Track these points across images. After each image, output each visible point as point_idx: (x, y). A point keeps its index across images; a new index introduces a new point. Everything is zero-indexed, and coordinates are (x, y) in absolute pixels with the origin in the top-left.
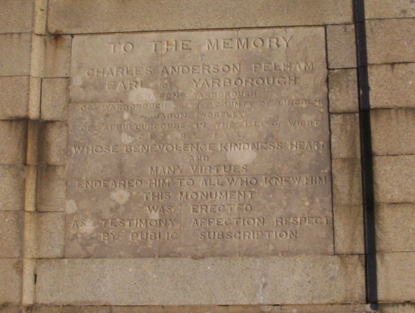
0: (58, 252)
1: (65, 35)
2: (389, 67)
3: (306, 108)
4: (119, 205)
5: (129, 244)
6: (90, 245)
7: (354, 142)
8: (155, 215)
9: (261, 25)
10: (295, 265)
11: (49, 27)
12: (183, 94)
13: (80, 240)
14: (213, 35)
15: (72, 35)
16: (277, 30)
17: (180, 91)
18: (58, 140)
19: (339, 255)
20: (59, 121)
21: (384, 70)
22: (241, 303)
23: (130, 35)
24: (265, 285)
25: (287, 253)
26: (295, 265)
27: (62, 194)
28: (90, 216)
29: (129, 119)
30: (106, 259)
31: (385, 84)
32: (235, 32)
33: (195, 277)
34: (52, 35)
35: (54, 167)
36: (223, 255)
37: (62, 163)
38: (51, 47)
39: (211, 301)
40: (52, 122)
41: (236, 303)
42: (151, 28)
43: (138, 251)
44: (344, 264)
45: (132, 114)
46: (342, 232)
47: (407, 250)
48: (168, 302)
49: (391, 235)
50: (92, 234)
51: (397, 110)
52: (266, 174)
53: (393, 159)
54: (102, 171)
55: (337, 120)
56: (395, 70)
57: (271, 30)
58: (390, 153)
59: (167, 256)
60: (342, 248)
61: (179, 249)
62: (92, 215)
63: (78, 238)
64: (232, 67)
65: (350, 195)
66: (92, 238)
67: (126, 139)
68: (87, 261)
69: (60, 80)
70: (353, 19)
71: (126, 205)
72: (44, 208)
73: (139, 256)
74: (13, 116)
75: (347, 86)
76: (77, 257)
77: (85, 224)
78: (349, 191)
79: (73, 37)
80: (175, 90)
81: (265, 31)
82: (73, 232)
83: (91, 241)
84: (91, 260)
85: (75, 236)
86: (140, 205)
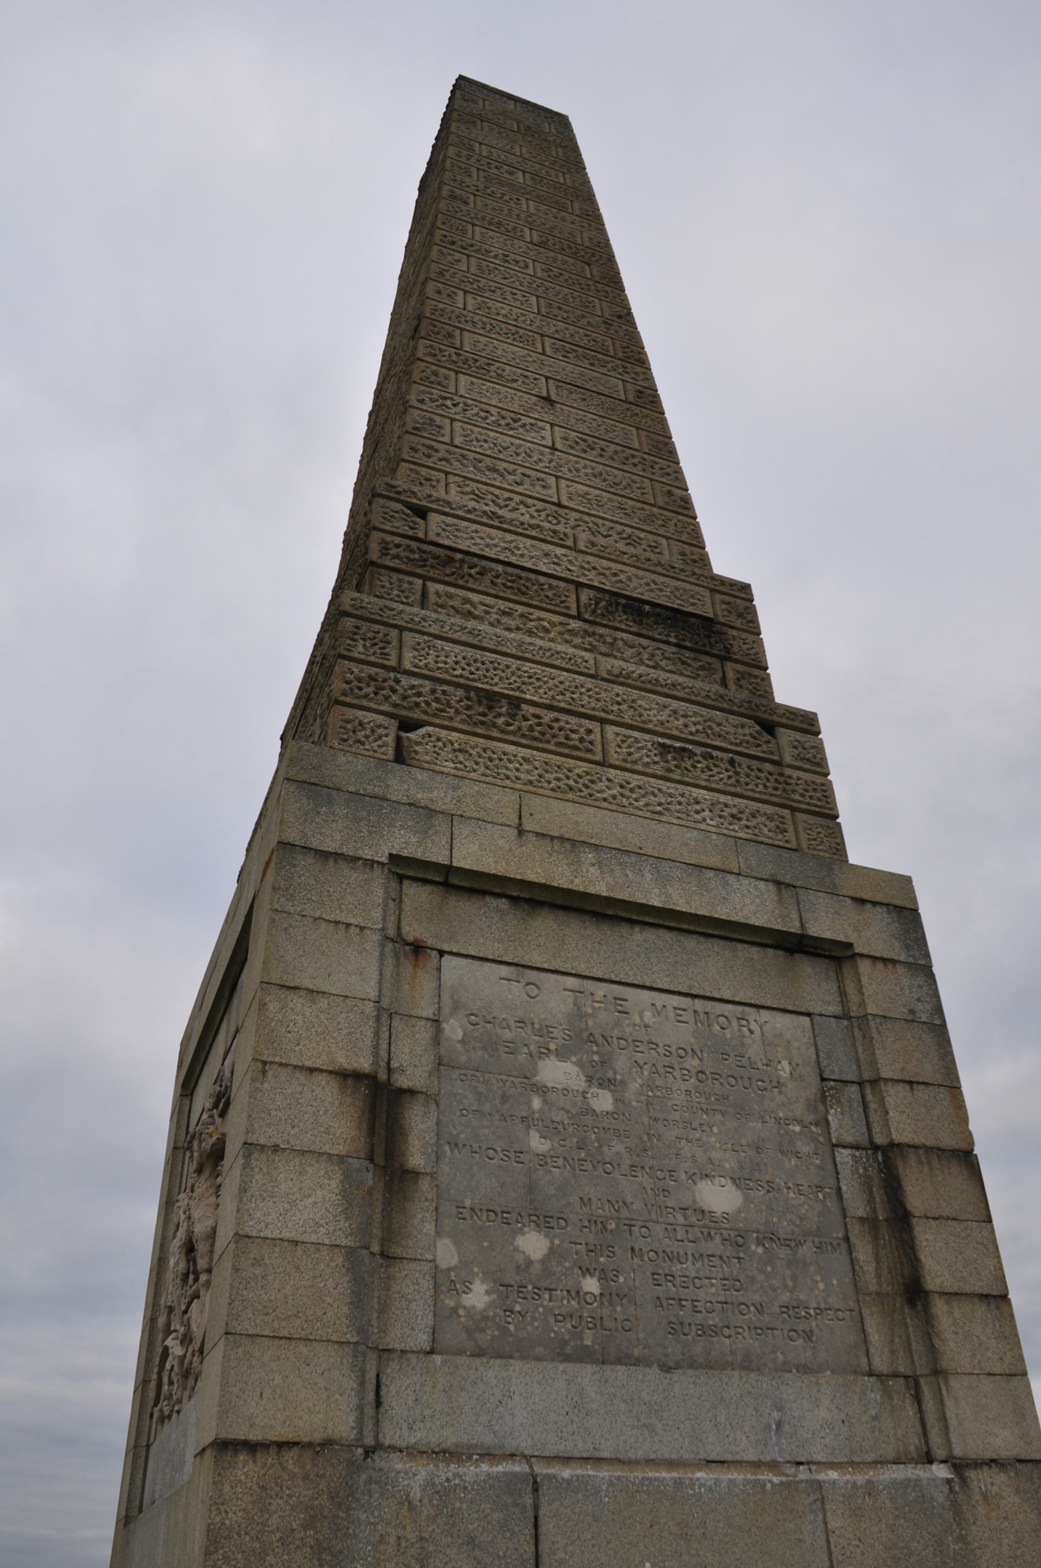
0: (423, 1340)
1: (432, 949)
2: (907, 1087)
3: (801, 1133)
4: (532, 1262)
5: (552, 1335)
6: (483, 1330)
7: (871, 1195)
8: (591, 1285)
9: (726, 997)
10: (819, 1391)
11: (404, 931)
12: (623, 1083)
13: (463, 1319)
14: (661, 999)
15: (442, 953)
16: (747, 1009)
17: (618, 1077)
18: (422, 1126)
19: (879, 1376)
20: (421, 1092)
21: (902, 1090)
22: (745, 1458)
23: (535, 973)
24: (779, 1424)
25: (804, 1369)
26: (819, 1391)
27: (429, 1227)
28: (481, 1275)
29: (541, 1111)
30: (512, 1361)
31: (907, 1110)
32: (689, 1000)
33: (668, 1405)
34: (408, 944)
35: (415, 1175)
36: (709, 1366)
37: (428, 1170)
38: (407, 967)
39: (698, 1453)
40: (412, 1092)
41: (738, 1457)
42: (567, 967)
43: (568, 1350)
44: (887, 1393)
45: (545, 1102)
46: (876, 1337)
47: (977, 1372)
48: (626, 1452)
49: (952, 1344)
50: (484, 1310)
51: (926, 1151)
52: (758, 1231)
53: (933, 1223)
54: (499, 1194)
55: (844, 1156)
56: (915, 1092)
57: (740, 1008)
58: (928, 1215)
59: (619, 1361)
60: (881, 1364)
61: (636, 1353)
62: (483, 1273)
63: (460, 1316)
64: (689, 1051)
65: (878, 1276)
66: (485, 1318)
67: (537, 1143)
68: (477, 1362)
69: (423, 1023)
70: (147, 1334)
71: (544, 1261)
72: (399, 1251)
73: (567, 1359)
74: (349, 1067)
75: (850, 1107)
76: (460, 1353)
77: (470, 1290)
78: (876, 1270)
79: (441, 956)
80: (610, 1074)
81: (730, 1007)
82: (450, 1302)
83: (483, 1324)
84: (485, 1360)
85: (454, 1310)
86: (567, 1264)
